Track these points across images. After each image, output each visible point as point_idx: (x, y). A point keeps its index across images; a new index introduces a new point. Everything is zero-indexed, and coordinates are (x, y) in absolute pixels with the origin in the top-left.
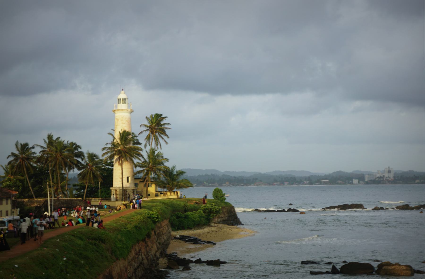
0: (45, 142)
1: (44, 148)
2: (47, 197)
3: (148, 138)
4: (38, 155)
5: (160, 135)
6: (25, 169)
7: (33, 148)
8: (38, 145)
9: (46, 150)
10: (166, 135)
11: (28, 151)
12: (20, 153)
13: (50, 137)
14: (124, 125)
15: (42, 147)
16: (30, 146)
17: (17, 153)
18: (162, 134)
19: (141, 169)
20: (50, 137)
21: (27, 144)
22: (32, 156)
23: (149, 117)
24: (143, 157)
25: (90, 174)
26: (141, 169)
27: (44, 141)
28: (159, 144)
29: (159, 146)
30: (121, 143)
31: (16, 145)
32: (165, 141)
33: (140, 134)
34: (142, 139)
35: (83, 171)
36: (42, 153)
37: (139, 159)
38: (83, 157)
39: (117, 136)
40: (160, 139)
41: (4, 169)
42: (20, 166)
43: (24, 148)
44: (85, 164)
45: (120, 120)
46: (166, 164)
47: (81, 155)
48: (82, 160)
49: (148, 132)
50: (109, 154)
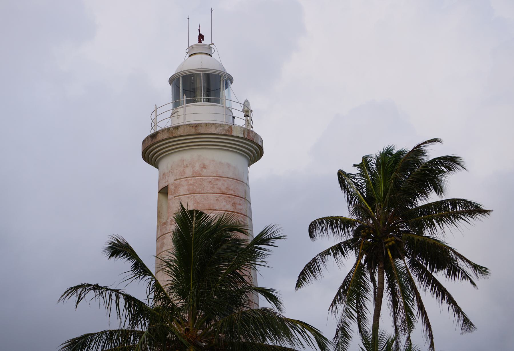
3: (351, 290)
28: (419, 323)
49: (350, 260)
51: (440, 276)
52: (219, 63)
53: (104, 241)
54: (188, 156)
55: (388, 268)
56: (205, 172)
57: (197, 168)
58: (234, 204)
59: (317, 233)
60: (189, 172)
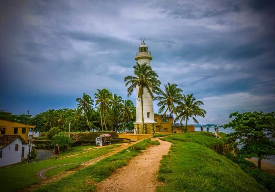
53: (97, 89)
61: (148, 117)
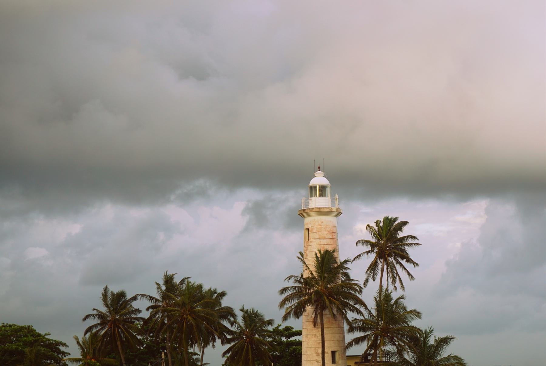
0: (159, 288)
1: (157, 300)
2: (125, 358)
3: (373, 267)
4: (146, 315)
5: (397, 261)
6: (119, 343)
7: (135, 298)
8: (143, 295)
9: (160, 304)
10: (408, 260)
11: (125, 307)
12: (110, 312)
13: (169, 280)
14: (324, 241)
15: (151, 298)
16: (129, 296)
17: (104, 310)
18: (403, 258)
19: (363, 334)
20: (169, 280)
21: (122, 295)
22: (133, 316)
23: (373, 225)
24: (366, 308)
25: (247, 350)
26: (363, 334)
27: (156, 286)
28: (397, 280)
29: (398, 284)
30: (320, 277)
31: (105, 296)
32: (409, 274)
33: (354, 259)
34: (357, 272)
35: (234, 345)
36: (151, 310)
37: (359, 312)
38: (232, 319)
39: (311, 261)
40: (399, 268)
41: (78, 343)
42: (111, 336)
43: (118, 302)
44: (238, 331)
45: (314, 231)
46: (415, 323)
47: (228, 313)
48: (232, 326)
49: (373, 256)
50: (295, 302)
51: (403, 262)
52: (230, 363)
54: (316, 218)
55: (386, 260)
56: (322, 224)
57: (320, 223)
58: (333, 236)
59: (358, 244)
60: (317, 224)
61: (334, 361)
